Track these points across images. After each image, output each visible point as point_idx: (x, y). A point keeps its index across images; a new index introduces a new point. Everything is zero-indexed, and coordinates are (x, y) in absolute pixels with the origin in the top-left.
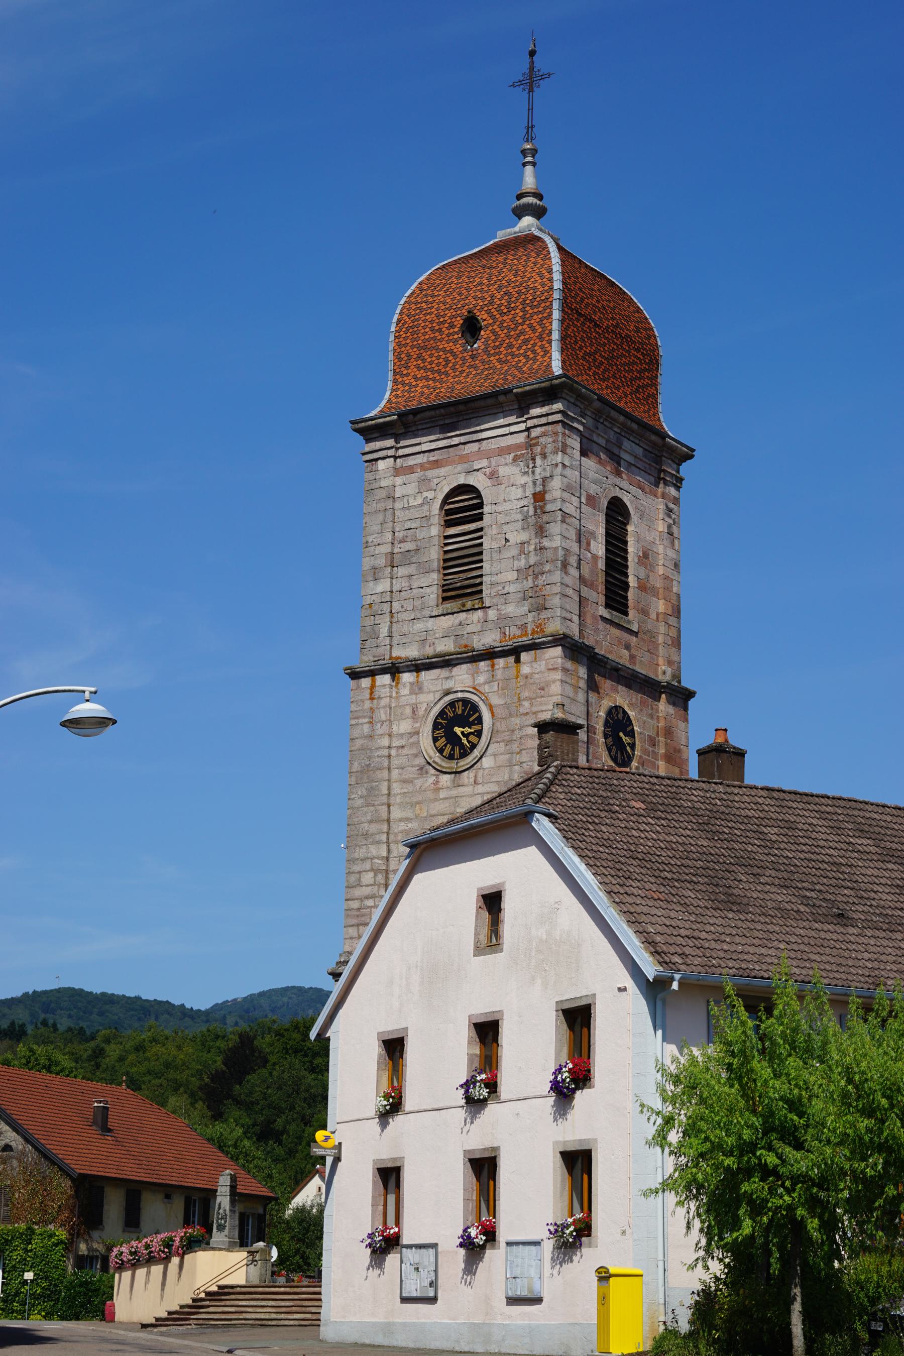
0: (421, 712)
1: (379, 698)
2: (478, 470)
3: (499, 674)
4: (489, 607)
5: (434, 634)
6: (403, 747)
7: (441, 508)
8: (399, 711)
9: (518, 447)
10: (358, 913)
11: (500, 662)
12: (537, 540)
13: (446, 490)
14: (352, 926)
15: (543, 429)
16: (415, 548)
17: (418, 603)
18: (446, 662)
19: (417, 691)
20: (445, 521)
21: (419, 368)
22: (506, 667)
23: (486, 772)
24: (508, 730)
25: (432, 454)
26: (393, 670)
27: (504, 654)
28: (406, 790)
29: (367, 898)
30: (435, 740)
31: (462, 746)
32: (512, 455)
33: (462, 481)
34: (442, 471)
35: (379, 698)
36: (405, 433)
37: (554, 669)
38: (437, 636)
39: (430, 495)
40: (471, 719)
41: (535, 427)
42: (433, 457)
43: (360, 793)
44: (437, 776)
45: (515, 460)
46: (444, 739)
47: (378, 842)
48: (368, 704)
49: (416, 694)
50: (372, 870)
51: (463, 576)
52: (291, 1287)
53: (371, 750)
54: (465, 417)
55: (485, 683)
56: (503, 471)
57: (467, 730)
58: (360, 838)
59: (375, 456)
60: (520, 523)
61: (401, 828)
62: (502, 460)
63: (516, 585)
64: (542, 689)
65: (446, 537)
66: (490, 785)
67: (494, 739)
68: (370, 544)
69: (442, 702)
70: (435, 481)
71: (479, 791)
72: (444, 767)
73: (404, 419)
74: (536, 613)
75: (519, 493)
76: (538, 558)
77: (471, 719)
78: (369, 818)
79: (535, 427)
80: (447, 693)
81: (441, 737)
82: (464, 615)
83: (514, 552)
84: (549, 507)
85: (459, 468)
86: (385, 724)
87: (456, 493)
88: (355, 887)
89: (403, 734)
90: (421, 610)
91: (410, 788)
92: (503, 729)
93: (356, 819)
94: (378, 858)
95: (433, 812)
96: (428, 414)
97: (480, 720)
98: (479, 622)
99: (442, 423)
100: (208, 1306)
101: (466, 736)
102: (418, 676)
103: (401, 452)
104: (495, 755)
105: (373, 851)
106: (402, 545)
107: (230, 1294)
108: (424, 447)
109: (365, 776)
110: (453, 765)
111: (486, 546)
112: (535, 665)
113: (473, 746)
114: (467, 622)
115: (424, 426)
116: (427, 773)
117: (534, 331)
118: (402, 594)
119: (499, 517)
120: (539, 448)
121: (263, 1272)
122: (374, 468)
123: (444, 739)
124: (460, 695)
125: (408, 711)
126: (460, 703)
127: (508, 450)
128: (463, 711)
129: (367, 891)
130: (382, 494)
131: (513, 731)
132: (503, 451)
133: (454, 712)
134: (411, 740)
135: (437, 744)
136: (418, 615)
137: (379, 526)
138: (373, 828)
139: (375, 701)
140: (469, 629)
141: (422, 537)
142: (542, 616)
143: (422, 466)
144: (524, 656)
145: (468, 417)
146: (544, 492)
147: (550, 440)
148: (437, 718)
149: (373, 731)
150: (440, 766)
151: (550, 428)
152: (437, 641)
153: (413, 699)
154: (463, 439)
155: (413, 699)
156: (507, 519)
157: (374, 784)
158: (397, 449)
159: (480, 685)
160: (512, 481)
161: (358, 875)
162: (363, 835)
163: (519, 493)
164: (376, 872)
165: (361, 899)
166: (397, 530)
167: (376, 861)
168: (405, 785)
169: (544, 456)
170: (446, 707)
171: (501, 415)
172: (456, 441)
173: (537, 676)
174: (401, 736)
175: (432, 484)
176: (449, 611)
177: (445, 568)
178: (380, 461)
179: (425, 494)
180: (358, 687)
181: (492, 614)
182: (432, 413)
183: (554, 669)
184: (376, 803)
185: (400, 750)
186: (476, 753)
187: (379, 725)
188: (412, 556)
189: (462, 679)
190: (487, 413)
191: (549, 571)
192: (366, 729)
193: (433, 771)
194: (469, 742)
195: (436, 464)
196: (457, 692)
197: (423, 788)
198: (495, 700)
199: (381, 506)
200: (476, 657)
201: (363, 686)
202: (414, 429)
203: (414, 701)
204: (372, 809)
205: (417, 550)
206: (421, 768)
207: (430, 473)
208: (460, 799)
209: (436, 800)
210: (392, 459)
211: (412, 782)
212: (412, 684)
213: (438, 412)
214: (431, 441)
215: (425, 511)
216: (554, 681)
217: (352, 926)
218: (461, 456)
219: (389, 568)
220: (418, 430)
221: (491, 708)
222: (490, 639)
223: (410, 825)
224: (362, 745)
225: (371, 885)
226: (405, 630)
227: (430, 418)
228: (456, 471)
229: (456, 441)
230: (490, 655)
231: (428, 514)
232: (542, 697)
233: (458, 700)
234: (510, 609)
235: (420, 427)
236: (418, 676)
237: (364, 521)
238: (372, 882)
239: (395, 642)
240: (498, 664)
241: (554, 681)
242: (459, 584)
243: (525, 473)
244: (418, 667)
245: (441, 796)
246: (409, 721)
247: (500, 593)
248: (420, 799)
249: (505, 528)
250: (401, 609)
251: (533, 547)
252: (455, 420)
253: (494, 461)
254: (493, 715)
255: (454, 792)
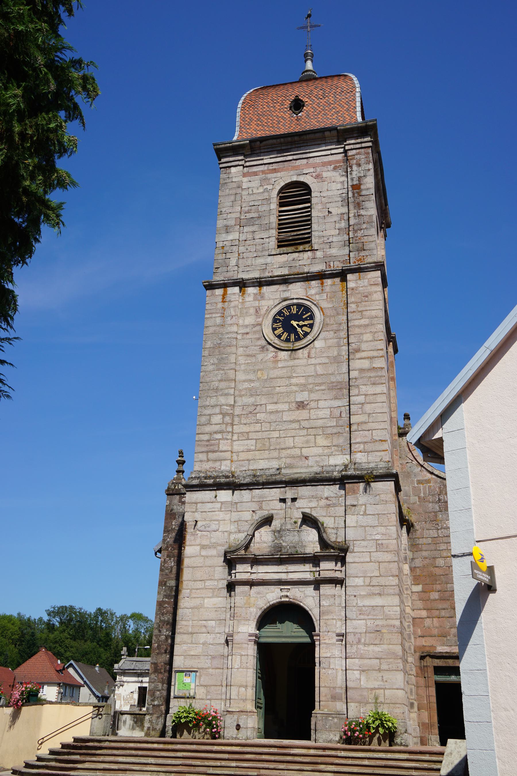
0: (263, 311)
1: (230, 301)
2: (307, 174)
3: (327, 289)
4: (317, 250)
5: (273, 265)
6: (247, 333)
7: (278, 195)
8: (245, 311)
9: (337, 161)
10: (207, 443)
11: (328, 282)
12: (356, 211)
13: (282, 184)
14: (202, 452)
15: (358, 151)
16: (257, 216)
17: (259, 248)
18: (285, 281)
19: (259, 298)
20: (280, 203)
21: (258, 125)
22: (334, 284)
23: (318, 350)
24: (336, 324)
25: (271, 165)
26: (241, 285)
27: (332, 276)
28: (249, 361)
29: (216, 433)
30: (274, 329)
31: (296, 333)
32: (333, 166)
33: (295, 179)
34: (279, 174)
35: (230, 301)
36: (251, 154)
37: (375, 284)
38: (275, 267)
39: (270, 187)
40: (304, 317)
41: (352, 149)
42: (271, 167)
43: (212, 362)
44: (276, 352)
45: (335, 169)
46: (281, 329)
47: (227, 395)
48: (220, 305)
49: (259, 300)
50: (221, 413)
51: (293, 234)
52: (165, 743)
53: (222, 334)
54: (297, 146)
55: (316, 294)
56: (325, 175)
57: (301, 323)
58: (211, 392)
59: (229, 164)
60: (340, 203)
61: (244, 387)
62: (325, 169)
63: (337, 238)
64: (367, 296)
65: (280, 212)
66: (321, 359)
67: (324, 329)
68: (223, 212)
69: (280, 305)
70: (273, 180)
71: (312, 363)
72: (282, 347)
73: (253, 144)
74: (357, 253)
75: (339, 186)
76: (357, 221)
77: (304, 317)
78: (219, 378)
79: (352, 149)
80: (285, 300)
81: (279, 328)
82: (297, 254)
83: (337, 219)
84: (363, 193)
85: (292, 173)
86: (234, 318)
87: (288, 187)
88: (205, 425)
89: (248, 325)
90: (262, 251)
91: (253, 360)
92: (331, 323)
93: (208, 379)
94: (227, 405)
95: (272, 376)
96: (270, 142)
97: (312, 317)
98: (308, 258)
99: (279, 148)
100: (84, 762)
101: (301, 327)
102: (260, 290)
103: (248, 164)
104: (325, 339)
105: (222, 400)
106: (247, 215)
107: (101, 748)
108: (265, 161)
109: (217, 351)
110: (290, 345)
111: (313, 214)
112: (359, 282)
113: (306, 334)
114: (299, 259)
115: (266, 150)
116: (267, 350)
117: (343, 107)
118: (246, 242)
119: (323, 199)
120: (355, 161)
121: (106, 724)
122: (228, 171)
123: (281, 329)
124: (295, 301)
125: (252, 311)
126: (295, 307)
127: (330, 163)
128: (298, 312)
129: (217, 428)
130: (235, 185)
131: (340, 324)
132: (324, 164)
133: (289, 312)
134: (254, 329)
135: (276, 332)
136: (260, 254)
137: (231, 203)
138: (223, 385)
139: (226, 303)
140: (301, 263)
141: (263, 210)
142: (360, 254)
143: (263, 172)
144: (349, 277)
145: (299, 145)
146: (360, 184)
147: (364, 157)
148: (275, 315)
149: (224, 322)
150: (279, 345)
151: (363, 150)
152: (274, 270)
153: (256, 304)
154: (295, 157)
155: (256, 304)
156: (330, 200)
157: (224, 356)
158: (246, 162)
159: (312, 295)
160: (333, 180)
161: (208, 417)
162: (214, 389)
163: (339, 186)
164: (224, 415)
165: (211, 434)
166: (243, 206)
167: (225, 407)
168: (248, 358)
169: (359, 165)
170: (283, 309)
171: (324, 145)
172: (290, 158)
173: (361, 289)
174: (247, 326)
175: (271, 181)
176: (285, 252)
177: (279, 229)
178: (232, 168)
179: (265, 187)
180: (213, 295)
181: (319, 254)
182: (275, 141)
183: (375, 284)
184: (225, 368)
185: (245, 336)
186: (309, 337)
187: (229, 318)
188: (255, 221)
189: (297, 291)
190: (313, 143)
191: (366, 228)
192: (218, 321)
193: (273, 349)
194: (303, 331)
195: (275, 171)
196: (293, 299)
197: (264, 360)
198: (324, 305)
199: (234, 192)
200: (308, 278)
201: (217, 294)
202: (258, 152)
203: (257, 305)
204: (222, 372)
205: (259, 217)
206: (263, 347)
207: (269, 176)
208: (295, 368)
209: (275, 368)
210: (242, 167)
211: (254, 356)
212: (255, 294)
213: (278, 140)
214: (271, 158)
215: (266, 195)
216: (376, 292)
217: (202, 452)
218: (294, 167)
219: (238, 226)
220: (261, 153)
221: (321, 309)
222: (317, 268)
223: (252, 385)
224: (215, 331)
225: (220, 424)
226: (249, 262)
227: (272, 145)
228: (290, 174)
229: (290, 158)
230: (321, 276)
231: (268, 197)
232: (366, 301)
233: (293, 305)
234: (334, 251)
235: (262, 151)
236: (260, 290)
237: (219, 200)
238: (221, 422)
239: (240, 270)
240: (327, 282)
241: (376, 292)
242: (291, 238)
243: (343, 175)
244: (260, 283)
245: (280, 366)
246: (254, 317)
247: (325, 242)
248: (262, 367)
249: (328, 205)
250: (246, 251)
251: (353, 214)
252: (289, 147)
253: (318, 169)
254: (324, 314)
255: (291, 363)
